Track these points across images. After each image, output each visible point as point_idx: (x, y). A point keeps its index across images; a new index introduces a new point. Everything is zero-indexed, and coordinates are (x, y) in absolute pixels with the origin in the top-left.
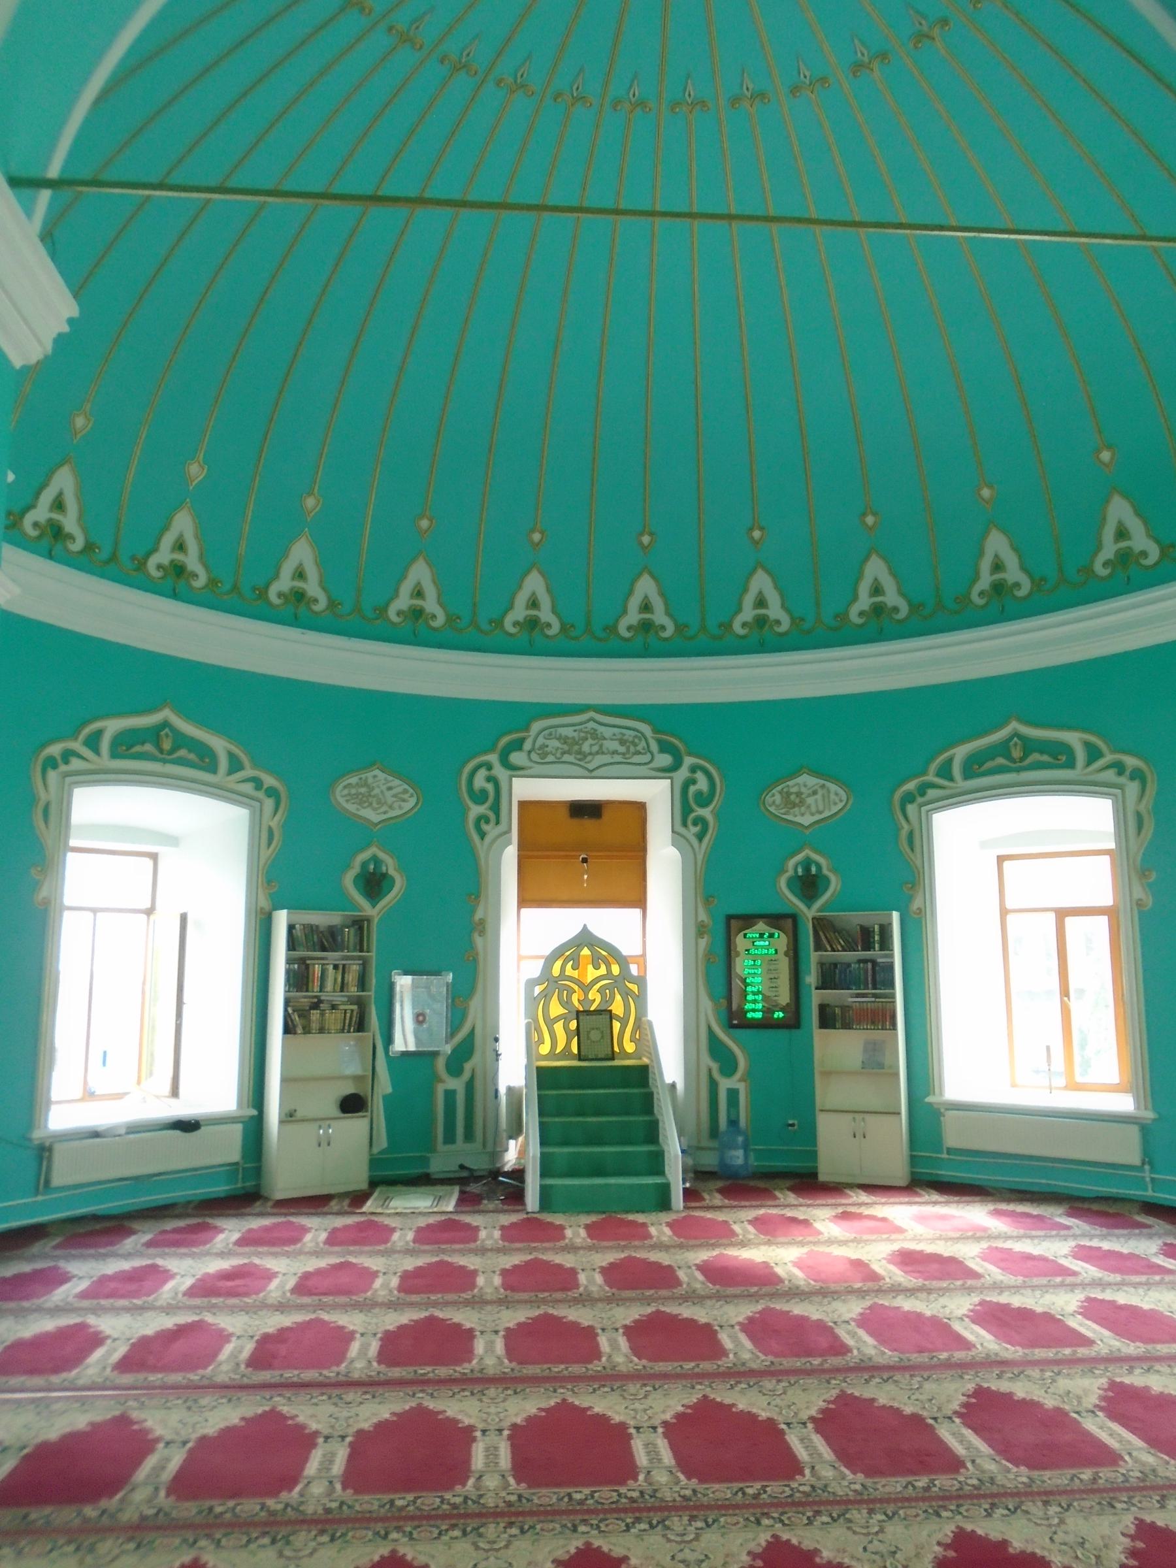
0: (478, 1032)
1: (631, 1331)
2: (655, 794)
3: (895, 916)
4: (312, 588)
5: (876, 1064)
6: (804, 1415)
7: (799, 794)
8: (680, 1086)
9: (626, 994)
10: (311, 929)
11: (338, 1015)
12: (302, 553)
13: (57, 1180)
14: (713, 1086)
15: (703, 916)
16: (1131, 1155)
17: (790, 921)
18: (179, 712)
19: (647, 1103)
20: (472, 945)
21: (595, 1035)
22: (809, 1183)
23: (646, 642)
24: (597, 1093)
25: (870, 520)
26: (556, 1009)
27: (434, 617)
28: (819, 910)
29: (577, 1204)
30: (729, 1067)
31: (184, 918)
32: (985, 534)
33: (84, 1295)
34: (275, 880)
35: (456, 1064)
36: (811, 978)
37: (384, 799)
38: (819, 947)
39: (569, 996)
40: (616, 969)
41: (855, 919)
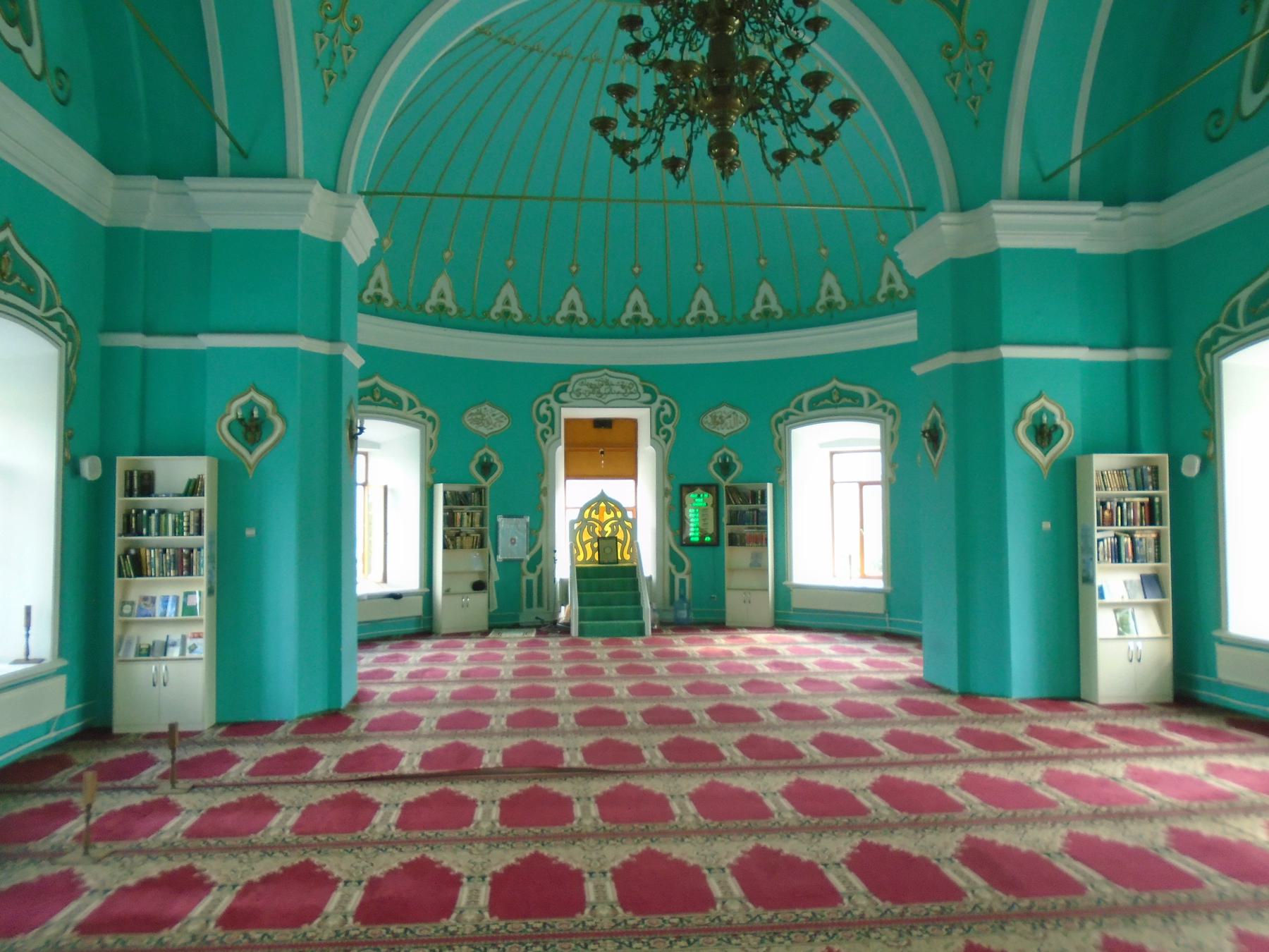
0: (544, 550)
1: (697, 798)
2: (643, 416)
3: (769, 487)
4: (449, 302)
5: (758, 565)
6: (838, 858)
8: (654, 578)
9: (625, 528)
10: (455, 494)
11: (470, 539)
12: (443, 283)
14: (672, 577)
15: (668, 485)
16: (878, 607)
19: (635, 585)
22: (719, 625)
23: (637, 329)
24: (608, 581)
25: (762, 262)
26: (586, 537)
28: (732, 481)
29: (596, 633)
30: (680, 566)
31: (386, 488)
32: (823, 275)
33: (193, 833)
34: (435, 468)
35: (532, 565)
36: (725, 519)
37: (492, 421)
38: (729, 502)
40: (619, 514)
41: (750, 487)
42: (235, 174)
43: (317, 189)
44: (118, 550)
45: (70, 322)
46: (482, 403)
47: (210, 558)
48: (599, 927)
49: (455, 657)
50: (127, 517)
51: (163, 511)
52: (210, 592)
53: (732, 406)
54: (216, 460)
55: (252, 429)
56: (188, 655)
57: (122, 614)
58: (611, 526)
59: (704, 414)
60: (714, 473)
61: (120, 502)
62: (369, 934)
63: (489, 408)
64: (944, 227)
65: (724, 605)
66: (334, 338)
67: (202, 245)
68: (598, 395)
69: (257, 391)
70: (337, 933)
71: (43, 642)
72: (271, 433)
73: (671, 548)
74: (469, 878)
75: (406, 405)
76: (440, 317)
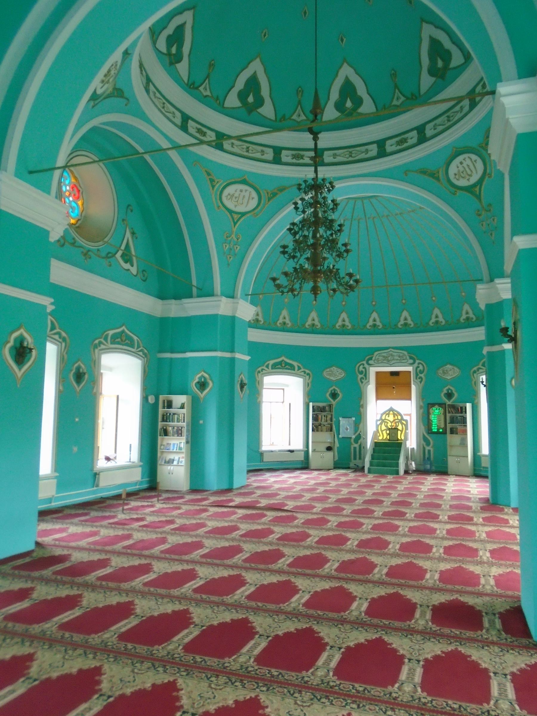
3: (469, 406)
7: (447, 371)
8: (415, 448)
9: (402, 424)
10: (318, 407)
13: (264, 460)
15: (421, 404)
17: (444, 406)
18: (287, 357)
20: (360, 410)
21: (393, 435)
23: (406, 329)
26: (384, 427)
27: (348, 326)
30: (428, 444)
34: (310, 395)
37: (336, 374)
39: (387, 423)
41: (461, 405)
42: (199, 296)
43: (224, 299)
44: (160, 427)
45: (146, 351)
46: (332, 367)
47: (188, 431)
48: (416, 628)
49: (391, 494)
50: (163, 416)
51: (174, 414)
52: (187, 442)
53: (451, 364)
54: (190, 397)
55: (202, 385)
56: (180, 464)
57: (161, 449)
58: (396, 423)
59: (438, 369)
60: (444, 398)
61: (161, 411)
62: (308, 612)
63: (335, 368)
64: (480, 291)
65: (447, 464)
66: (232, 351)
67: (188, 320)
68: (388, 361)
69: (205, 372)
70: (294, 609)
71: (135, 457)
72: (208, 387)
73: (424, 435)
74: (410, 660)
75: (296, 368)
76: (313, 330)
